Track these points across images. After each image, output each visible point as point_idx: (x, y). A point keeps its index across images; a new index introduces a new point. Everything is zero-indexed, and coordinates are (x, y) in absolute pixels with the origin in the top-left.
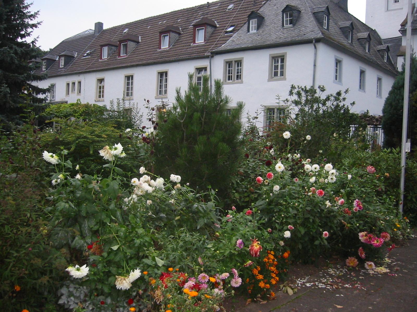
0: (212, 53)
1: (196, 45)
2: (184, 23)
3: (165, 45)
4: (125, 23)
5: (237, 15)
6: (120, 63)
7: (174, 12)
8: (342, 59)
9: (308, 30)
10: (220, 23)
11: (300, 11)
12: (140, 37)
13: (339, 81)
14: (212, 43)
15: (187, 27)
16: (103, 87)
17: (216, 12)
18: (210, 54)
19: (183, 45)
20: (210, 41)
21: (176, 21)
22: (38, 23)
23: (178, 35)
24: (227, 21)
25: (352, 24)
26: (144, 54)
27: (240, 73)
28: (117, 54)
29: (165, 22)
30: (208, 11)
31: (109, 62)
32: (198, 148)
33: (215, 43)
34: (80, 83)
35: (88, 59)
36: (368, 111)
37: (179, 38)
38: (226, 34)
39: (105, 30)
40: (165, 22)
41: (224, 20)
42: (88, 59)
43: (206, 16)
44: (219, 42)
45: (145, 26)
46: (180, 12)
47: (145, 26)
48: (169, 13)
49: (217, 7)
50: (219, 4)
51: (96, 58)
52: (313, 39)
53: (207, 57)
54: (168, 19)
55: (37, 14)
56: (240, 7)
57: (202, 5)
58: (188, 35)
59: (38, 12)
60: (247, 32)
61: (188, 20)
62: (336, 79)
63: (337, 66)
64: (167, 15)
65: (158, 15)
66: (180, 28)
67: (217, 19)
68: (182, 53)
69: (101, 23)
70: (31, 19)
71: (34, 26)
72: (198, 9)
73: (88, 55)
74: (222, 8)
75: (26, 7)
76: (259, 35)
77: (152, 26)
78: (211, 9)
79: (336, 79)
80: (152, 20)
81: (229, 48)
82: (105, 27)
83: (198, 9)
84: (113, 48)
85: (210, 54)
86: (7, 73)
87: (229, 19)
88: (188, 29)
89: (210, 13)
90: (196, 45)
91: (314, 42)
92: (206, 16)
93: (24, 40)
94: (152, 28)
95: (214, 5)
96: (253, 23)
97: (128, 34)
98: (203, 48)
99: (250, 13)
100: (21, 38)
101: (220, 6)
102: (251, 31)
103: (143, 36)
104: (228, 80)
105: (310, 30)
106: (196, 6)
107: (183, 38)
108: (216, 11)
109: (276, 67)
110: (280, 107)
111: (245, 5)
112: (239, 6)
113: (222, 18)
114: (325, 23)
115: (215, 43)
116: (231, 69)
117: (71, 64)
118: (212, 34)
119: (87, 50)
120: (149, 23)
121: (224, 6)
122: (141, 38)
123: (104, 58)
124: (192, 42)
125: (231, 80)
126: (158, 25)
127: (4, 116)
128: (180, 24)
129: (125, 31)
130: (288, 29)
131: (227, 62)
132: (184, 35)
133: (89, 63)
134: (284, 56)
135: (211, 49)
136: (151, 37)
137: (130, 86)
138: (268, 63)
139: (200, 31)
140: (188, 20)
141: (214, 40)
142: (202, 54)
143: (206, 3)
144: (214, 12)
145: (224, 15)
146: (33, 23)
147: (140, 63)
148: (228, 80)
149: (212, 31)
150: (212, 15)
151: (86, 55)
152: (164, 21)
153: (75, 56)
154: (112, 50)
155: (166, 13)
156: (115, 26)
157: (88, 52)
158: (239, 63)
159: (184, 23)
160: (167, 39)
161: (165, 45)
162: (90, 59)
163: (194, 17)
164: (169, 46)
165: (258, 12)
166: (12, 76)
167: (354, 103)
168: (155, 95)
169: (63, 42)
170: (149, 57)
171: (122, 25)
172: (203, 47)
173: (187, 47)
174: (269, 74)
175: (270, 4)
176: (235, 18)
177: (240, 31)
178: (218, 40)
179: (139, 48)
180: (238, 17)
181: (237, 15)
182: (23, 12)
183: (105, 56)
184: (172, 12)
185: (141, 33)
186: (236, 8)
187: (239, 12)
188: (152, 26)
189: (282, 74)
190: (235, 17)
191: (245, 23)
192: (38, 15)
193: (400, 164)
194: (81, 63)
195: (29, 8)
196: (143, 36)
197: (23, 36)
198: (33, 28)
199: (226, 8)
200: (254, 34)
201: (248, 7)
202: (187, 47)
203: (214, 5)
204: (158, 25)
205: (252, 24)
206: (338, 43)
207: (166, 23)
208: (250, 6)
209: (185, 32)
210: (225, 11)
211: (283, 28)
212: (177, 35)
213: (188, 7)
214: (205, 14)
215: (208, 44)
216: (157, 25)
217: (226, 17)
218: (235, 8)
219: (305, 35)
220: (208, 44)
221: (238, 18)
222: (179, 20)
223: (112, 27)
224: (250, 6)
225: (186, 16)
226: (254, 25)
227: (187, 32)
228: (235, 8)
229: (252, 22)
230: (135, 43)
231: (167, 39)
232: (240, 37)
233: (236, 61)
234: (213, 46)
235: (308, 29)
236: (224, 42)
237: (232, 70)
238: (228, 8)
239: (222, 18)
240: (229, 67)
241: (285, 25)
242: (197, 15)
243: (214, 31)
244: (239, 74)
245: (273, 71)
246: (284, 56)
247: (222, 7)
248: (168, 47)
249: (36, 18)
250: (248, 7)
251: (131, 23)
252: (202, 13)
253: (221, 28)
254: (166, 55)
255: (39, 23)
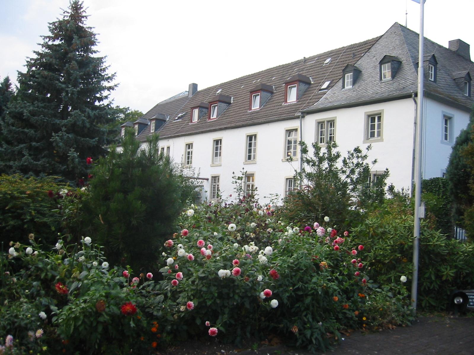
0: (302, 113)
1: (287, 104)
2: (278, 81)
3: (256, 106)
4: (219, 84)
5: (334, 70)
6: (209, 126)
7: (270, 69)
8: (454, 115)
9: (409, 83)
10: (315, 80)
11: (402, 62)
12: (232, 97)
13: (449, 141)
14: (304, 102)
15: (281, 86)
16: (192, 152)
17: (312, 67)
18: (300, 114)
19: (274, 105)
20: (302, 100)
21: (270, 79)
22: (115, 85)
23: (270, 94)
24: (322, 77)
25: (468, 74)
26: (234, 116)
27: (333, 134)
28: (207, 117)
29: (259, 80)
30: (304, 67)
31: (199, 125)
32: (113, 205)
33: (308, 101)
34: (169, 148)
35: (178, 123)
36: (387, 169)
37: (271, 98)
38: (320, 92)
39: (199, 91)
40: (259, 80)
41: (320, 76)
42: (178, 123)
43: (301, 72)
44: (312, 101)
45: (239, 85)
46: (276, 69)
47: (239, 85)
48: (264, 71)
49: (314, 62)
50: (316, 59)
51: (187, 122)
52: (412, 93)
53: (298, 117)
54: (263, 77)
55: (114, 76)
56: (337, 61)
57: (298, 60)
58: (281, 94)
59: (115, 73)
60: (342, 88)
61: (283, 78)
62: (446, 139)
63: (446, 124)
64: (262, 72)
65: (253, 73)
66: (273, 87)
67: (312, 75)
68: (272, 113)
69: (196, 84)
70: (108, 82)
71: (109, 89)
72: (294, 65)
73: (179, 118)
74: (319, 63)
75: (104, 70)
76: (354, 91)
77: (246, 86)
78: (308, 64)
79: (446, 139)
80: (246, 79)
81: (321, 106)
82: (199, 89)
83: (294, 65)
84: (204, 110)
85: (300, 114)
86: (79, 138)
87: (325, 75)
88: (281, 88)
89: (306, 69)
90: (287, 104)
91: (413, 96)
92: (301, 72)
93: (101, 103)
94: (246, 88)
95: (311, 60)
96: (349, 77)
97: (220, 95)
98: (294, 108)
99: (344, 68)
100: (99, 102)
101: (317, 61)
102: (346, 87)
103: (235, 97)
104: (320, 143)
105: (410, 82)
106: (292, 62)
107: (275, 97)
108: (312, 66)
109: (373, 127)
110: (377, 173)
111: (343, 58)
112: (336, 60)
113: (317, 74)
114: (432, 74)
115: (308, 101)
116: (323, 130)
117: (161, 128)
118: (305, 92)
119: (179, 113)
120: (243, 82)
121: (321, 60)
122: (233, 98)
123: (195, 121)
124: (283, 102)
125: (324, 142)
126: (252, 84)
127: (73, 181)
128: (273, 83)
129: (218, 92)
130: (386, 83)
131: (319, 123)
132: (277, 94)
133: (179, 127)
134: (380, 114)
135: (302, 108)
136: (243, 97)
137: (219, 151)
138: (363, 122)
139: (293, 89)
140: (283, 78)
141: (307, 98)
142: (292, 114)
143: (303, 58)
144: (310, 68)
145: (320, 70)
146: (110, 86)
147: (229, 126)
148: (320, 143)
149: (306, 89)
150: (307, 71)
151: (177, 118)
152: (258, 79)
153: (167, 120)
154: (203, 113)
155: (261, 71)
156: (209, 87)
157: (180, 115)
158: (332, 123)
159: (278, 81)
160: (258, 98)
161: (256, 106)
162: (181, 123)
163: (289, 74)
164: (260, 107)
165: (355, 65)
166: (83, 140)
167: (375, 161)
168: (243, 160)
169: (157, 105)
170: (238, 120)
171: (216, 86)
172: (295, 107)
173: (277, 107)
174: (365, 135)
175: (369, 56)
176: (331, 73)
177: (335, 88)
178: (310, 98)
179: (230, 110)
180: (334, 71)
181: (334, 70)
182: (101, 75)
183: (196, 119)
184: (267, 70)
185: (234, 93)
186: (334, 62)
187: (336, 67)
188: (246, 86)
189: (379, 135)
190: (331, 72)
191: (340, 79)
192: (115, 77)
193: (412, 233)
194: (172, 127)
195: (106, 70)
196: (235, 97)
197: (100, 99)
198: (110, 91)
199: (323, 62)
200: (349, 89)
201: (346, 61)
202: (277, 107)
203: (311, 60)
204: (252, 84)
205: (348, 79)
206: (448, 97)
207: (260, 82)
208: (349, 59)
209: (278, 91)
210: (322, 66)
211: (381, 82)
212: (269, 94)
213: (284, 63)
214: (301, 70)
215: (300, 103)
216: (251, 85)
217: (322, 72)
218: (332, 62)
219: (404, 89)
220: (300, 103)
221: (334, 73)
222: (274, 78)
223: (207, 88)
224: (349, 59)
225: (281, 74)
226: (349, 80)
227: (280, 90)
228: (332, 62)
229: (348, 76)
230: (226, 105)
231: (258, 98)
232: (334, 94)
233: (328, 122)
234: (305, 105)
235: (408, 81)
236: (317, 100)
237: (324, 131)
238: (325, 63)
239: (317, 74)
240: (322, 128)
241: (383, 79)
242: (292, 72)
243: (308, 88)
244: (332, 136)
245: (370, 131)
246: (380, 114)
247: (318, 62)
248: (258, 107)
249: (113, 80)
250: (346, 61)
251: (225, 83)
252: (298, 69)
253: (315, 85)
254: (255, 116)
255: (116, 86)
